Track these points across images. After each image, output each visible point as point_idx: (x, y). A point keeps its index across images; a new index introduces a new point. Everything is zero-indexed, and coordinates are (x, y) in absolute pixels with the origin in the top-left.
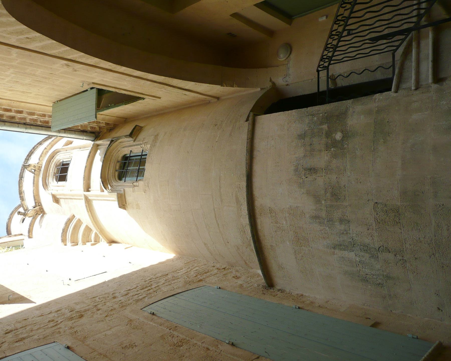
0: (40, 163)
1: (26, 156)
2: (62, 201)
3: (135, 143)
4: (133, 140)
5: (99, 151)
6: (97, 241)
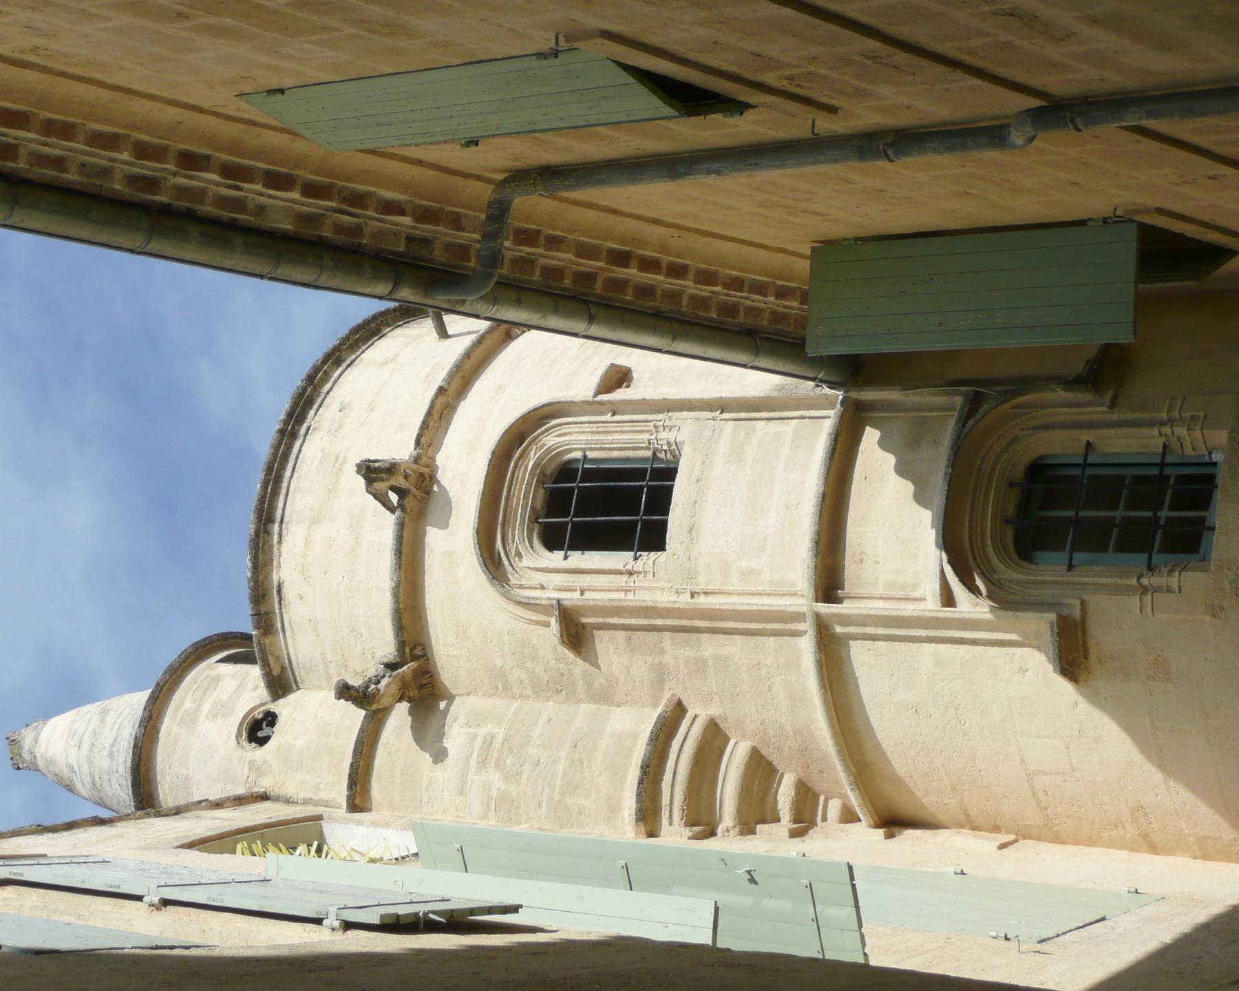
0: (424, 460)
1: (282, 416)
2: (607, 646)
3: (1115, 416)
5: (871, 436)
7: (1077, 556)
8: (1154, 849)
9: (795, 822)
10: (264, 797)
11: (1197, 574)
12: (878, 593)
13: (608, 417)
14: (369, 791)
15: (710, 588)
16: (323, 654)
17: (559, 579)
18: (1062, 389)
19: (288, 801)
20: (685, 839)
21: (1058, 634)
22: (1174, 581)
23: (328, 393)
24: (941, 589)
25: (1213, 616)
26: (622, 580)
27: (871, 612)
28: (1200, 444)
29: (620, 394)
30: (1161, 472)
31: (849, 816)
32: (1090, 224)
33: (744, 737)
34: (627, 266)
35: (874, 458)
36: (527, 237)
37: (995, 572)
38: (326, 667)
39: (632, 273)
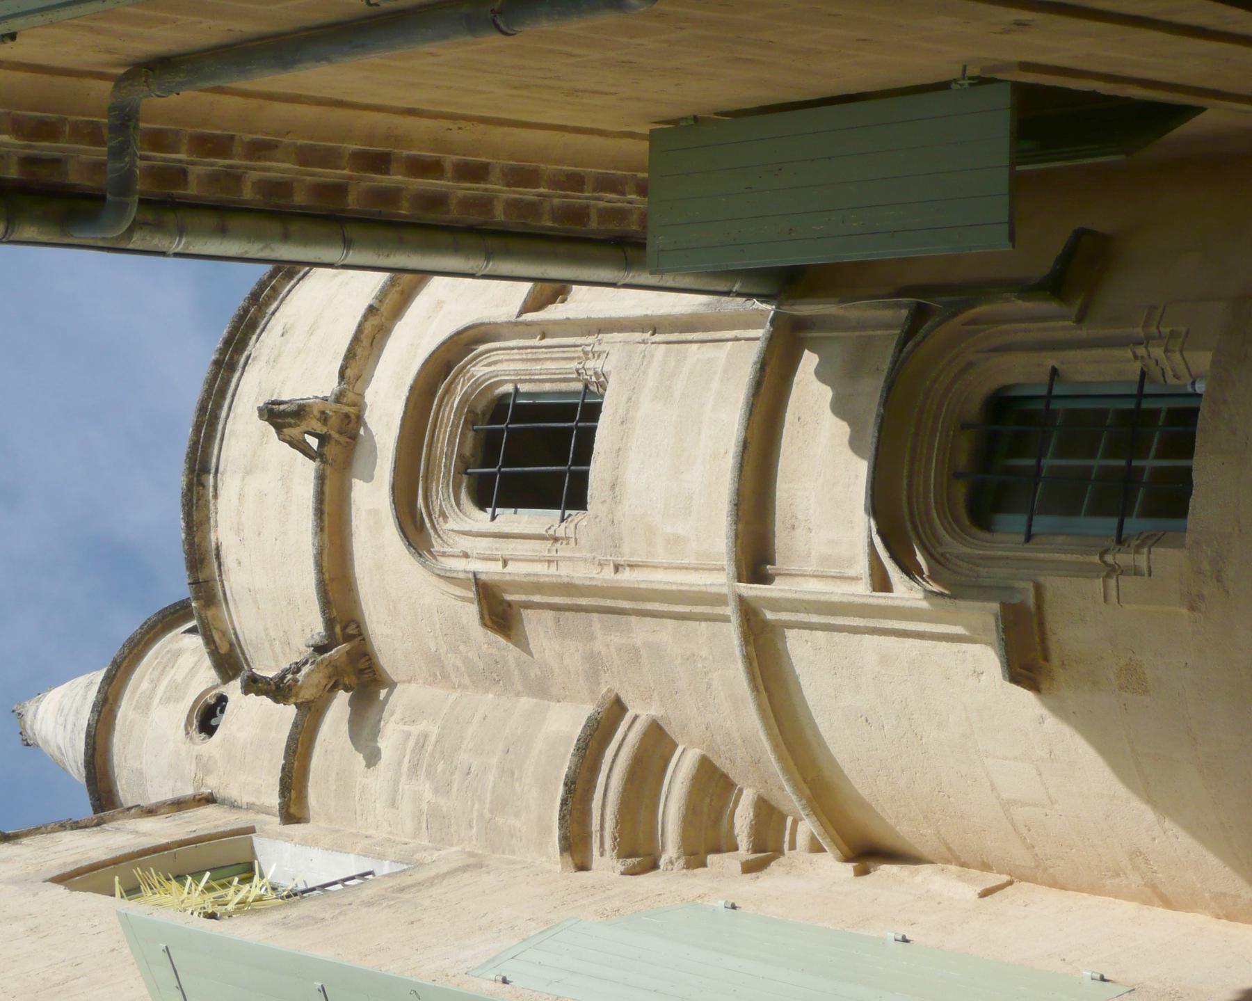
0: (350, 397)
1: (219, 345)
2: (535, 625)
3: (1083, 333)
4: (1074, 309)
5: (809, 360)
6: (768, 846)
7: (1041, 523)
8: (1167, 902)
9: (755, 851)
10: (210, 800)
11: (1170, 551)
12: (809, 569)
13: (536, 342)
14: (306, 797)
15: (634, 559)
16: (266, 629)
17: (482, 545)
18: (1019, 298)
19: (234, 806)
20: (617, 874)
21: (1004, 630)
22: (1142, 560)
23: (273, 313)
24: (872, 568)
25: (1192, 608)
26: (543, 548)
27: (798, 596)
28: (1182, 369)
29: (555, 312)
30: (1139, 404)
31: (816, 848)
32: (954, 86)
33: (692, 744)
34: (387, 172)
35: (810, 391)
36: (159, 140)
37: (941, 544)
38: (272, 645)
39: (395, 179)
